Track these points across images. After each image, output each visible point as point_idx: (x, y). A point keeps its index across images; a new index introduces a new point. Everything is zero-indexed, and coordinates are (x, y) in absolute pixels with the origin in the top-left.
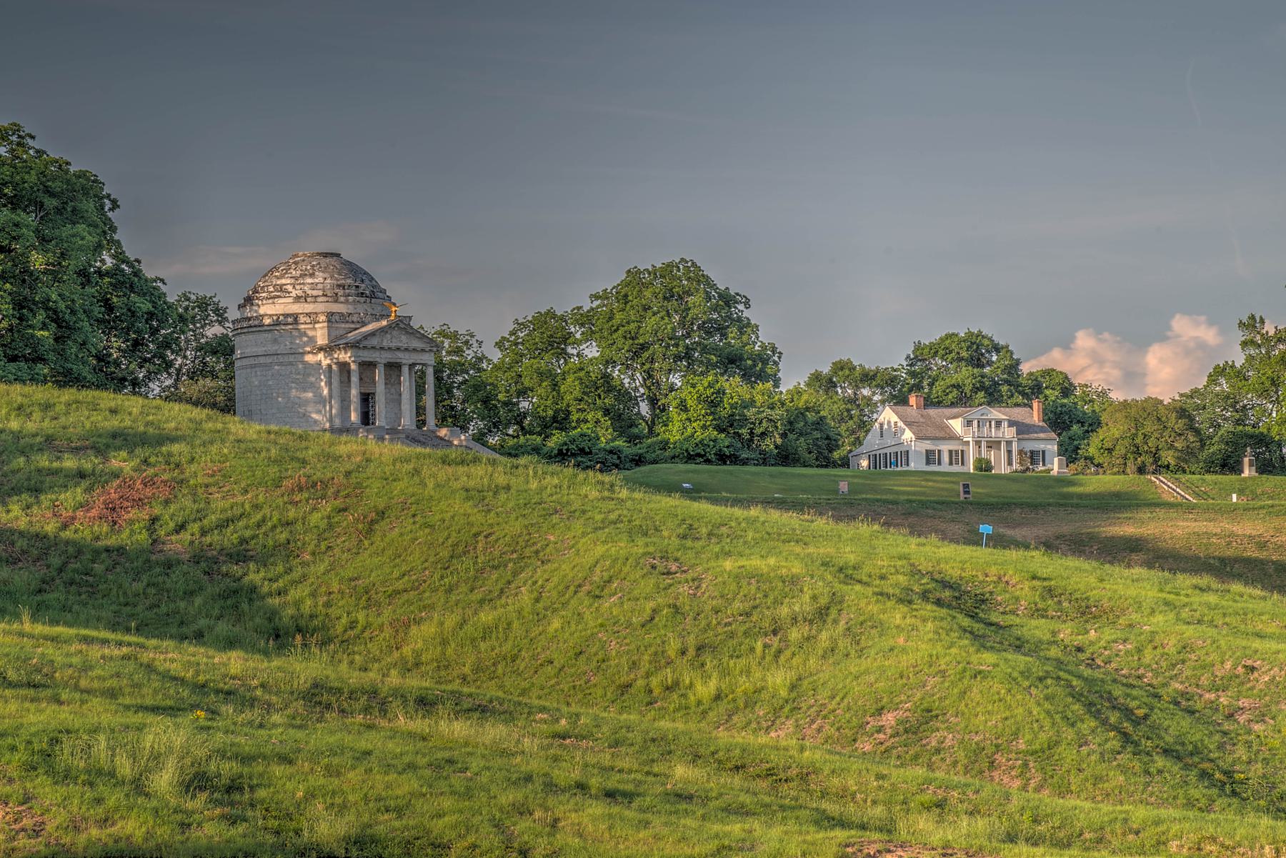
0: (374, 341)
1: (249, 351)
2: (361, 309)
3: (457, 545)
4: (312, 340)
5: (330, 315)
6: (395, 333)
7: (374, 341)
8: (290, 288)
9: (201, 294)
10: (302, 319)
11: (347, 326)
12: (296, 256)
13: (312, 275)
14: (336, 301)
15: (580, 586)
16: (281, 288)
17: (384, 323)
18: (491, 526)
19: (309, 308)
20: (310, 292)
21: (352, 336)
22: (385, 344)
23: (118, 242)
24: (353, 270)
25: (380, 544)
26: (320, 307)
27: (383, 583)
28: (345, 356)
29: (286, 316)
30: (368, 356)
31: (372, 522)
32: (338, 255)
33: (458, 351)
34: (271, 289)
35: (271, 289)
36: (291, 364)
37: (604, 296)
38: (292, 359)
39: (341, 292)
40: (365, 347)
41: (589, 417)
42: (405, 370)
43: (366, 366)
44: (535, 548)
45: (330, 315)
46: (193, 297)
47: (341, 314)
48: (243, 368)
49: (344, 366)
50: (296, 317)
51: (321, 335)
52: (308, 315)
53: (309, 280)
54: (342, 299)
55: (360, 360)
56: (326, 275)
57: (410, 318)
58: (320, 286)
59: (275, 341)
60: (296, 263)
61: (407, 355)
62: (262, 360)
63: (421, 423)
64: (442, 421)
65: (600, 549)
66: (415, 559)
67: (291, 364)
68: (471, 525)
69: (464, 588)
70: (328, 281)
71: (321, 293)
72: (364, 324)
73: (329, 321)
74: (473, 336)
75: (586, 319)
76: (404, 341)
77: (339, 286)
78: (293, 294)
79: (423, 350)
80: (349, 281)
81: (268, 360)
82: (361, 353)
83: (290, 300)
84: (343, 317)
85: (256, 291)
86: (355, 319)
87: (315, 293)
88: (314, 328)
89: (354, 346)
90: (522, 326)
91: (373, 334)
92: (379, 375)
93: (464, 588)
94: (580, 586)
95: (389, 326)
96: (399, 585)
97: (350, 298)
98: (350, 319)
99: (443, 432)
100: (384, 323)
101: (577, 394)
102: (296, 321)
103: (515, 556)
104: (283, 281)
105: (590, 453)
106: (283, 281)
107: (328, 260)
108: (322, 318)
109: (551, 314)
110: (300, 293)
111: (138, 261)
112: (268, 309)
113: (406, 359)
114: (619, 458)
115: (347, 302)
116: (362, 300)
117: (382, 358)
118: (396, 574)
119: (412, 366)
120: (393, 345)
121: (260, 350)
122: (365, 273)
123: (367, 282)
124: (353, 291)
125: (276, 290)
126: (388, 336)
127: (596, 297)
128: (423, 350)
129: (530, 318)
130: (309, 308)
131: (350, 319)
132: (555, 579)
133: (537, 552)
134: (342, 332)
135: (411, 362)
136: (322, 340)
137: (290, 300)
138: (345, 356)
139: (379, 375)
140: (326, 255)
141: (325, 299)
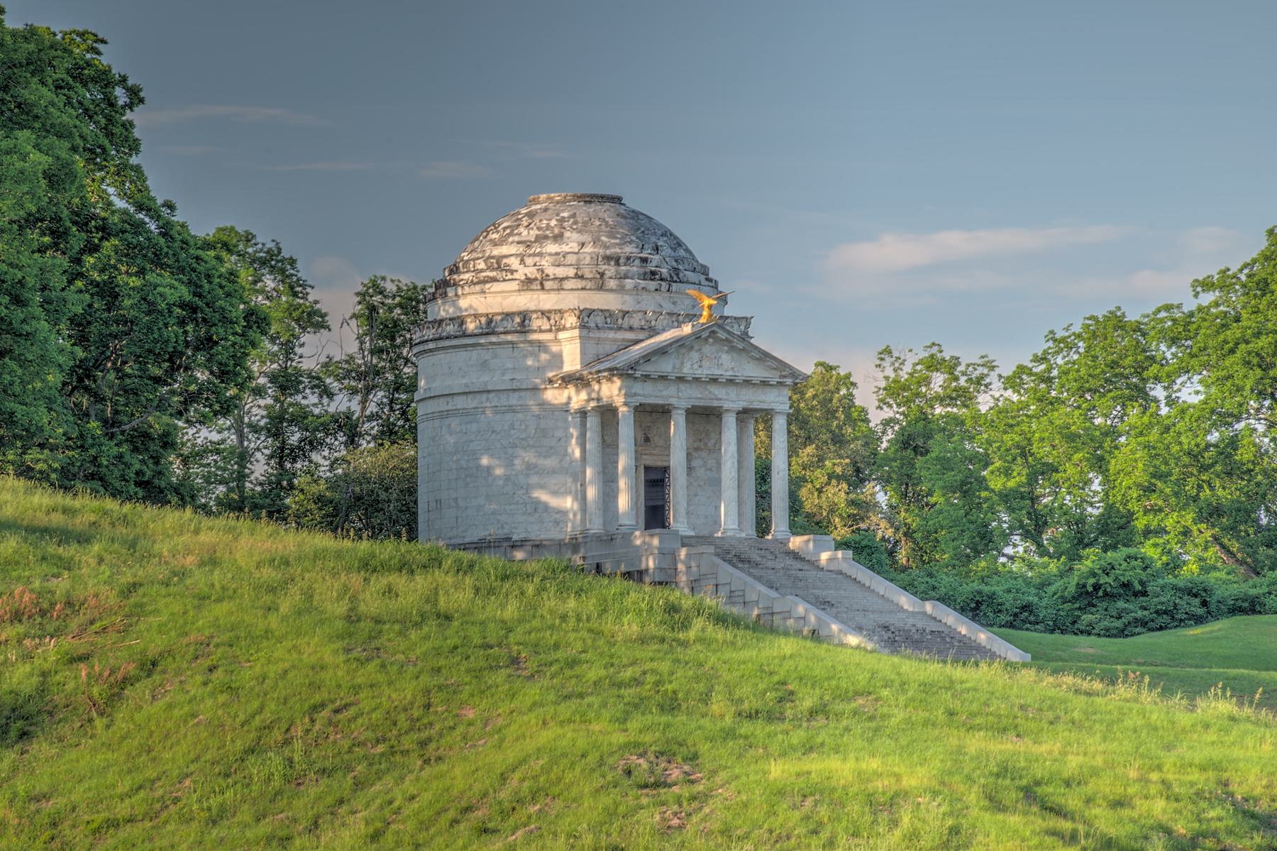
0: (666, 366)
1: (439, 386)
2: (650, 303)
3: (269, 727)
4: (558, 359)
5: (585, 316)
6: (708, 349)
7: (666, 366)
8: (514, 263)
9: (405, 281)
10: (537, 323)
11: (621, 335)
12: (535, 201)
13: (558, 238)
14: (601, 288)
15: (468, 809)
16: (498, 264)
17: (687, 329)
18: (356, 689)
19: (547, 301)
20: (551, 271)
21: (622, 359)
22: (687, 370)
23: (137, 169)
24: (640, 226)
25: (121, 725)
26: (571, 300)
27: (94, 804)
28: (612, 391)
29: (508, 316)
30: (652, 394)
31: (127, 681)
32: (617, 200)
33: (961, 396)
34: (481, 265)
35: (481, 265)
36: (511, 409)
37: (1224, 282)
38: (514, 400)
39: (610, 270)
40: (646, 377)
41: (1169, 523)
42: (730, 423)
43: (652, 416)
44: (424, 735)
45: (585, 316)
46: (390, 287)
47: (608, 314)
48: (430, 417)
49: (607, 413)
50: (525, 316)
51: (571, 351)
52: (545, 314)
53: (551, 248)
54: (612, 284)
55: (637, 401)
56: (586, 237)
57: (747, 320)
58: (571, 259)
59: (484, 365)
60: (531, 215)
61: (732, 392)
62: (460, 403)
63: (763, 526)
64: (795, 529)
65: (545, 736)
66: (174, 757)
67: (511, 409)
68: (315, 686)
69: (245, 814)
70: (588, 249)
71: (571, 272)
72: (653, 332)
73: (583, 327)
74: (992, 368)
75: (1182, 329)
76: (726, 364)
77: (608, 258)
78: (520, 275)
79: (765, 383)
80: (629, 249)
81: (470, 403)
82: (638, 387)
83: (514, 286)
84: (611, 319)
85: (454, 270)
86: (636, 321)
87: (561, 272)
88: (556, 340)
89: (627, 373)
90: (1064, 344)
91: (662, 351)
92: (677, 429)
93: (245, 814)
94: (468, 809)
95: (696, 336)
96: (122, 810)
97: (629, 283)
98: (626, 322)
99: (796, 542)
100: (687, 329)
101: (1140, 476)
102: (524, 329)
103: (381, 748)
104: (504, 250)
105: (1145, 594)
106: (504, 250)
107: (592, 208)
108: (571, 320)
109: (1117, 322)
110: (532, 272)
111: (170, 206)
112: (474, 302)
113: (732, 400)
114: (1204, 603)
115: (621, 289)
116: (653, 285)
117: (681, 398)
118: (125, 785)
119: (744, 415)
120: (703, 372)
121: (457, 384)
122: (667, 234)
123: (666, 251)
124: (635, 268)
125: (490, 268)
126: (695, 355)
127: (1207, 285)
128: (765, 383)
129: (1077, 329)
130: (547, 301)
131: (626, 322)
132: (427, 796)
133: (423, 744)
134: (609, 348)
135: (740, 405)
136: (572, 361)
137: (514, 286)
138: (612, 391)
139: (677, 429)
140: (603, 199)
141: (580, 284)
